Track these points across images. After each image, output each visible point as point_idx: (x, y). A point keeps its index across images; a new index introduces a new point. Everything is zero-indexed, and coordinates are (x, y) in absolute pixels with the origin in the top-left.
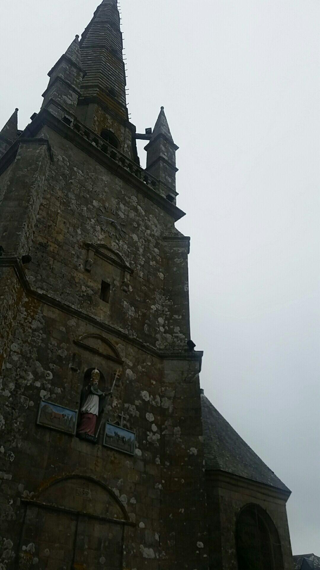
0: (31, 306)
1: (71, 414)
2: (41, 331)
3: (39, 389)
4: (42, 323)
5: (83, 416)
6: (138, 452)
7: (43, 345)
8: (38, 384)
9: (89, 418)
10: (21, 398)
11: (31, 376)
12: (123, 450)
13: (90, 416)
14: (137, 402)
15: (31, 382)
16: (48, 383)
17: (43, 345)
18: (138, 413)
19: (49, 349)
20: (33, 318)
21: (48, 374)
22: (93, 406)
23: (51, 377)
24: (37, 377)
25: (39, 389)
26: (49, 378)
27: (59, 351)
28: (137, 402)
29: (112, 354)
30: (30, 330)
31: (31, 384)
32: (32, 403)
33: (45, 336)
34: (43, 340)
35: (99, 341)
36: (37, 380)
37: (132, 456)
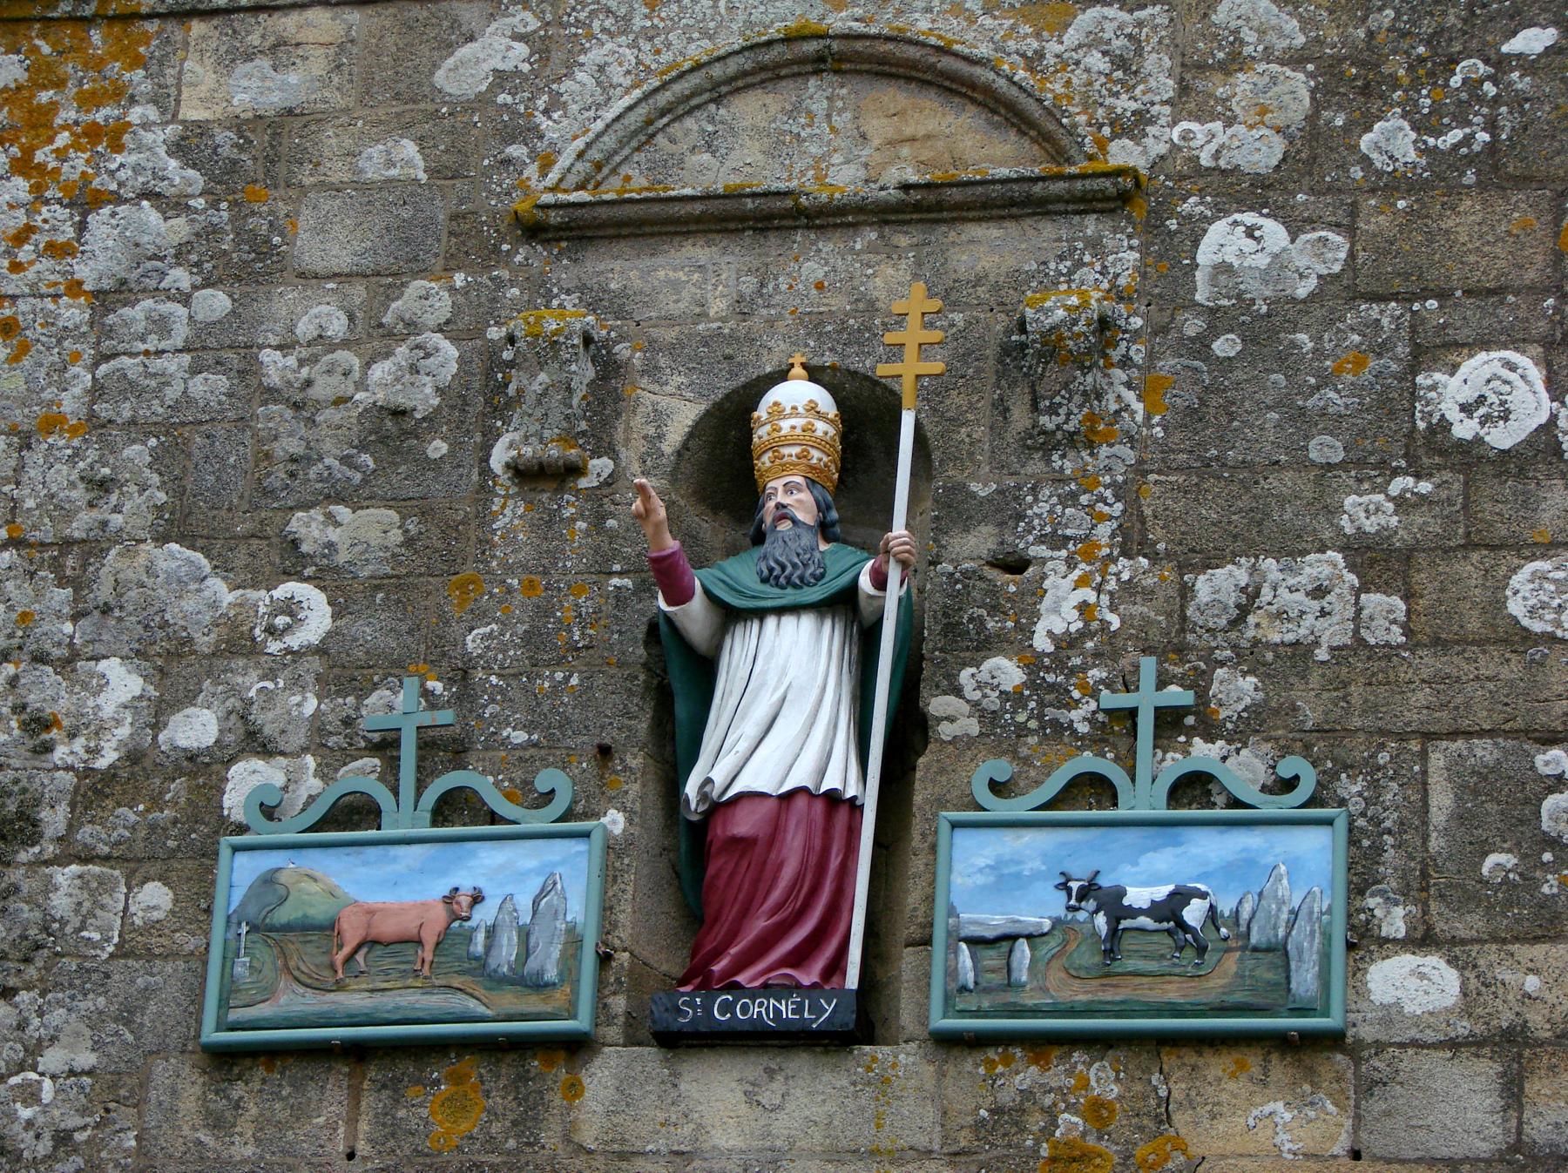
0: (53, 107)
1: (539, 886)
2: (180, 277)
3: (204, 770)
4: (171, 205)
5: (702, 856)
6: (1412, 985)
7: (210, 387)
8: (196, 728)
9: (743, 844)
10: (49, 887)
11: (122, 683)
12: (1035, 1012)
13: (744, 824)
14: (1366, 510)
15: (124, 732)
16: (296, 683)
17: (210, 387)
18: (1384, 607)
19: (271, 394)
20: (86, 201)
21: (290, 608)
22: (783, 716)
23: (317, 619)
24: (174, 666)
25: (204, 770)
26: (294, 641)
27: (379, 371)
28: (1366, 510)
29: (995, 155)
30: (73, 313)
31: (133, 756)
32: (155, 897)
33: (216, 302)
34: (203, 349)
35: (817, 94)
36: (190, 698)
37: (1333, 1040)
